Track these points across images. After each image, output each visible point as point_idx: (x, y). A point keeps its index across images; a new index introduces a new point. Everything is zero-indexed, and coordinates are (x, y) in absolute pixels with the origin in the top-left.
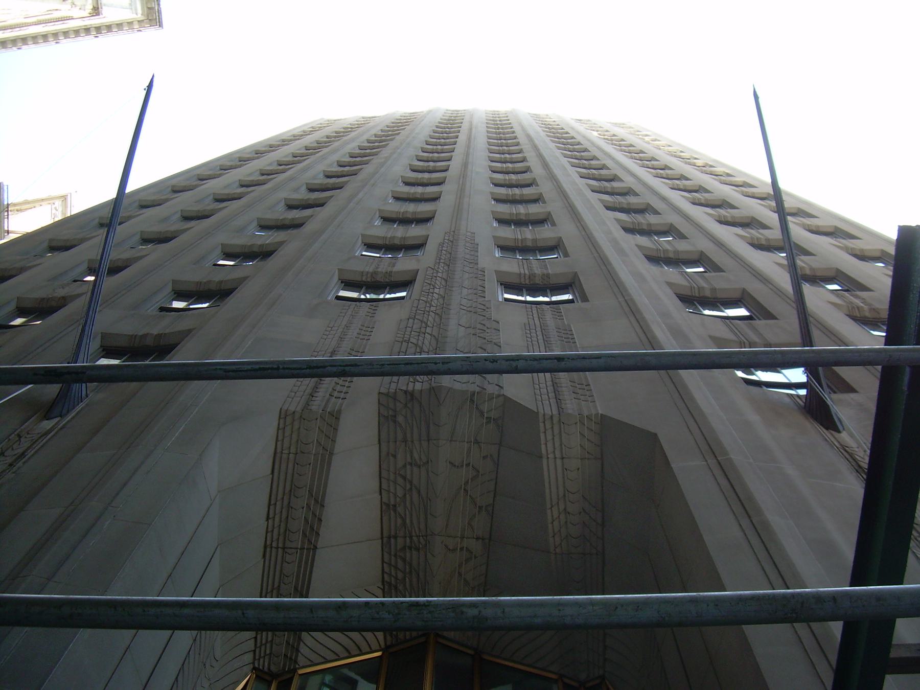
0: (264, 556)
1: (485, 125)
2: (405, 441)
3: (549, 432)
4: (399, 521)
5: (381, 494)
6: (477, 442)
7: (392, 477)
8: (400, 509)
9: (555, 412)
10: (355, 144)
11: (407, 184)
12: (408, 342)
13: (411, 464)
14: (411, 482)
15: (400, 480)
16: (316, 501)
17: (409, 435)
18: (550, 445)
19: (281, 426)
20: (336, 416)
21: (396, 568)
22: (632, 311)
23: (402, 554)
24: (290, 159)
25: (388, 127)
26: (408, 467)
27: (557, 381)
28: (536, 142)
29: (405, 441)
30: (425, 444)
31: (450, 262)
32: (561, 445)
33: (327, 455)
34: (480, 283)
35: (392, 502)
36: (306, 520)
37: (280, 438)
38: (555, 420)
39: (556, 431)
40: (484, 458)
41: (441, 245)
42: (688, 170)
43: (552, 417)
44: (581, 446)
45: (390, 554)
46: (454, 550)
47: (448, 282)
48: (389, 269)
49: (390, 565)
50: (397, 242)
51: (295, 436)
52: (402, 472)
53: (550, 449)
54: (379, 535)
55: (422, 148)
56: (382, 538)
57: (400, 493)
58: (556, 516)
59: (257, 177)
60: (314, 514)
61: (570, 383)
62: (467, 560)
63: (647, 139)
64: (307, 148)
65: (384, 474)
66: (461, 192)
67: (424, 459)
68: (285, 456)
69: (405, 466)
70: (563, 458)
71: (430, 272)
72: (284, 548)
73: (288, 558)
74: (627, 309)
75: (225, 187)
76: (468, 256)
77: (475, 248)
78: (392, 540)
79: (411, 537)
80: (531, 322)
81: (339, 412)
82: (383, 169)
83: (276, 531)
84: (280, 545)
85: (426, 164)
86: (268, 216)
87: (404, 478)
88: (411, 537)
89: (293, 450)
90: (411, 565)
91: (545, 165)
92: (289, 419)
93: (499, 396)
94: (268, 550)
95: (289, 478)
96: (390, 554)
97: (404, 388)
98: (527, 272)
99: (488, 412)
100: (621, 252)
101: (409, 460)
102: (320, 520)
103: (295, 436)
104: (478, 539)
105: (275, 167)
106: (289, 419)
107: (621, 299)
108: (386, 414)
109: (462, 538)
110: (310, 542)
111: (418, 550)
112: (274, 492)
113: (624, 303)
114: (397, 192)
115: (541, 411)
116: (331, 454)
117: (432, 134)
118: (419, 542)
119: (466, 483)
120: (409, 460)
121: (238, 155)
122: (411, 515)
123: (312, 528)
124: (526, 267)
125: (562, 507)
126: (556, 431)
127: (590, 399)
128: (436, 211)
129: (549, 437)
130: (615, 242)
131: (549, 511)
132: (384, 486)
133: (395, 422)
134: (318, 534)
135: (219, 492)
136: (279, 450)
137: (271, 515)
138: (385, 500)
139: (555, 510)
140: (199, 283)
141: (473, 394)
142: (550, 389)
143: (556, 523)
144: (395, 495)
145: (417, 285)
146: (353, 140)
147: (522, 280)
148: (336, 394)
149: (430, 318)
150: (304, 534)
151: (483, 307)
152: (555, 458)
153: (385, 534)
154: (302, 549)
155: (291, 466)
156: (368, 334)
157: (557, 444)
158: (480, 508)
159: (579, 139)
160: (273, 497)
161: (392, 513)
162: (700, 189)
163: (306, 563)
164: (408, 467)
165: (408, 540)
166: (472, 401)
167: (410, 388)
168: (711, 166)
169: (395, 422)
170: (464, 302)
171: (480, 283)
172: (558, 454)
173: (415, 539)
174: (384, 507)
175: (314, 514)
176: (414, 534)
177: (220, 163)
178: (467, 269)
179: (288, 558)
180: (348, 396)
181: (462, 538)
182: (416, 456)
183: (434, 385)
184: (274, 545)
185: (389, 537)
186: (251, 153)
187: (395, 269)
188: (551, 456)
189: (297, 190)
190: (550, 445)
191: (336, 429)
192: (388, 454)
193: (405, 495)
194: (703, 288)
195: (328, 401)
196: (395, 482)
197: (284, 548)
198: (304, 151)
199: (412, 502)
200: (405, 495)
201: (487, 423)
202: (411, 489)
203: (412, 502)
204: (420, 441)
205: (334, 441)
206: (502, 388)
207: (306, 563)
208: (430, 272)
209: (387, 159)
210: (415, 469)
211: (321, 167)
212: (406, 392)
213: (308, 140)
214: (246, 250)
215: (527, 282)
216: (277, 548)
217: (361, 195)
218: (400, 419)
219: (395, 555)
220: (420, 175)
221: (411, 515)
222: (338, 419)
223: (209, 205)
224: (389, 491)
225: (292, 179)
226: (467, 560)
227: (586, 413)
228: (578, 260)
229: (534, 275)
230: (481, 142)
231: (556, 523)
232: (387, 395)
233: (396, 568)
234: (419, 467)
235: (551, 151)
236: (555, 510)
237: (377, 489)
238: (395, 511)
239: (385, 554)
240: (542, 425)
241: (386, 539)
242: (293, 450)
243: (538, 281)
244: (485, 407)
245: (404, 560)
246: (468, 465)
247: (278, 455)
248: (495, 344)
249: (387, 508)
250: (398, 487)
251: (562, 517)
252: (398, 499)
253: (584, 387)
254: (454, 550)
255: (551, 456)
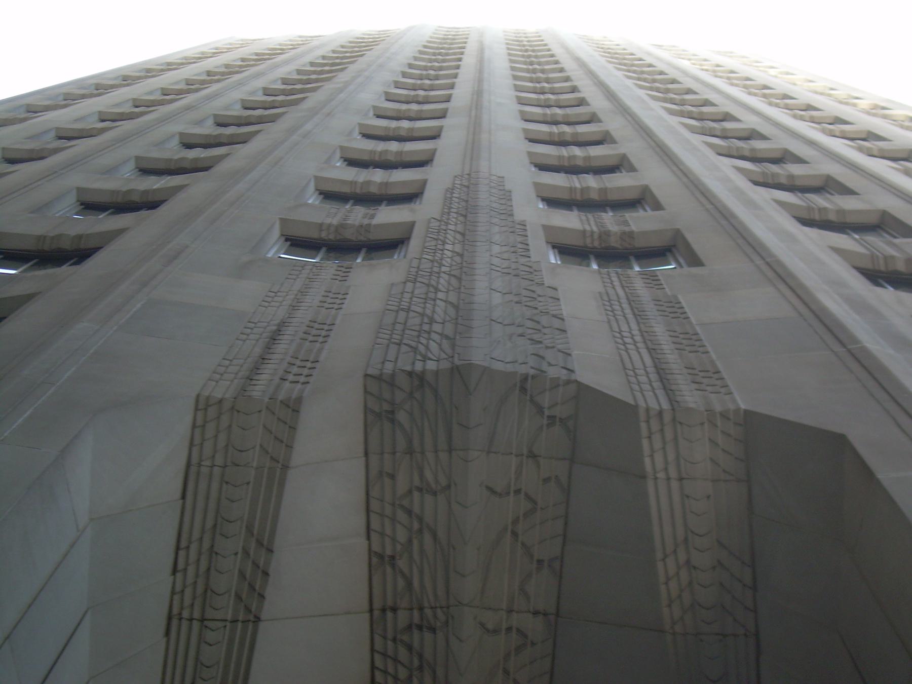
0: (167, 633)
1: (504, 46)
2: (410, 451)
3: (657, 438)
4: (401, 583)
5: (368, 538)
6: (533, 456)
7: (388, 510)
8: (402, 563)
9: (665, 405)
10: (292, 67)
11: (352, 162)
12: (408, 310)
13: (420, 490)
14: (420, 519)
15: (401, 516)
16: (260, 543)
17: (416, 443)
18: (659, 458)
19: (199, 422)
20: (294, 407)
21: (396, 660)
22: (780, 276)
23: (405, 638)
24: (182, 86)
25: (343, 47)
26: (416, 494)
27: (664, 366)
28: (593, 68)
29: (410, 451)
30: (443, 456)
31: (468, 211)
32: (678, 458)
33: (277, 471)
34: (519, 239)
35: (389, 552)
36: (242, 575)
37: (197, 441)
38: (667, 417)
39: (669, 435)
40: (546, 480)
41: (451, 190)
42: (845, 112)
43: (660, 413)
44: (711, 459)
45: (385, 638)
46: (496, 632)
47: (467, 237)
48: (366, 221)
49: (384, 655)
50: (374, 190)
51: (222, 437)
52: (405, 503)
53: (659, 464)
54: (366, 606)
55: (386, 93)
56: (371, 611)
57: (402, 535)
58: (672, 570)
59: (127, 109)
60: (256, 565)
61: (685, 371)
62: (518, 649)
63: (772, 72)
64: (209, 73)
65: (375, 505)
66: (476, 126)
67: (443, 482)
68: (204, 470)
69: (410, 492)
70: (681, 479)
71: (435, 224)
72: (202, 620)
73: (210, 636)
74: (770, 274)
75: (76, 120)
76: (494, 205)
77: (507, 196)
78: (389, 615)
79: (421, 609)
80: (611, 291)
81: (299, 400)
82: (342, 96)
83: (188, 592)
84: (197, 614)
85: (394, 124)
86: (155, 154)
87: (409, 512)
88: (421, 609)
89: (219, 460)
90: (421, 656)
91: (610, 95)
92: (212, 412)
93: (568, 382)
94: (175, 622)
95: (212, 505)
96: (385, 638)
97: (408, 368)
98: (595, 229)
99: (549, 408)
100: (751, 204)
101: (417, 482)
102: (266, 574)
103: (222, 437)
104: (536, 613)
105: (157, 96)
106: (212, 412)
107: (758, 261)
108: (377, 409)
109: (510, 611)
110: (248, 610)
111: (433, 630)
112: (186, 528)
113: (765, 268)
114: (368, 125)
115: (642, 403)
116: (285, 467)
117: (418, 55)
118: (435, 616)
119: (515, 522)
120: (417, 482)
121: (95, 81)
122: (421, 573)
123: (252, 587)
124: (592, 223)
125: (682, 557)
126: (669, 435)
127: (723, 390)
128: (435, 150)
129: (658, 445)
130: (738, 193)
131: (660, 565)
132: (375, 524)
133: (393, 421)
134: (262, 596)
135: (92, 520)
136: (195, 460)
137: (181, 566)
138: (376, 547)
139: (670, 561)
140: (41, 238)
141: (525, 378)
142: (654, 377)
143: (673, 584)
144: (394, 540)
145: (415, 244)
146: (287, 62)
147: (588, 241)
148: (291, 377)
149: (442, 281)
150: (238, 597)
151: (527, 269)
152: (668, 479)
153: (377, 604)
154: (235, 621)
155: (215, 486)
156: (338, 301)
157: (671, 457)
158: (540, 562)
159: (661, 67)
160: (185, 536)
161: (389, 570)
162: (871, 136)
163: (242, 644)
164: (416, 494)
165: (416, 613)
166: (523, 390)
167: (419, 367)
168: (884, 108)
169: (393, 421)
170: (496, 261)
171: (519, 239)
172: (673, 473)
173: (428, 612)
174: (375, 560)
175: (256, 565)
176: (426, 605)
177: (64, 90)
178: (494, 220)
179: (210, 636)
180: (311, 379)
181: (510, 611)
182: (428, 475)
183: (457, 362)
184: (186, 614)
185: (384, 610)
186: (116, 78)
187: (375, 221)
188: (661, 475)
189: (200, 122)
190: (659, 458)
191: (293, 428)
192: (381, 473)
193: (410, 541)
194: (893, 257)
195: (278, 387)
196: (393, 520)
197: (202, 620)
198: (204, 77)
199: (422, 551)
200: (410, 541)
201: (549, 425)
202: (420, 531)
203: (422, 551)
204: (436, 451)
205: (290, 447)
206: (572, 371)
207: (242, 644)
208: (435, 224)
209: (347, 84)
210: (428, 498)
211: (238, 95)
212: (410, 374)
213: (210, 64)
214: (120, 200)
215: (596, 244)
216: (191, 620)
217: (308, 127)
218: (402, 416)
219: (394, 640)
220: (381, 146)
221: (421, 573)
222: (296, 411)
223: (48, 143)
224: (382, 534)
225: (189, 108)
226: (518, 649)
227: (718, 408)
228: (678, 211)
229: (608, 233)
230: (500, 66)
231: (673, 584)
232: (379, 378)
233: (396, 660)
234: (435, 494)
235: (616, 79)
236: (670, 561)
237: (363, 530)
238: (393, 566)
239: (376, 637)
240: (643, 425)
241: (379, 613)
242: (219, 460)
243: (614, 242)
244: (545, 400)
245: (410, 648)
246: (517, 492)
247: (193, 469)
248: (554, 316)
249: (379, 561)
250: (398, 526)
251: (684, 574)
252: (399, 547)
253: (710, 374)
254: (496, 632)
255: (661, 475)
